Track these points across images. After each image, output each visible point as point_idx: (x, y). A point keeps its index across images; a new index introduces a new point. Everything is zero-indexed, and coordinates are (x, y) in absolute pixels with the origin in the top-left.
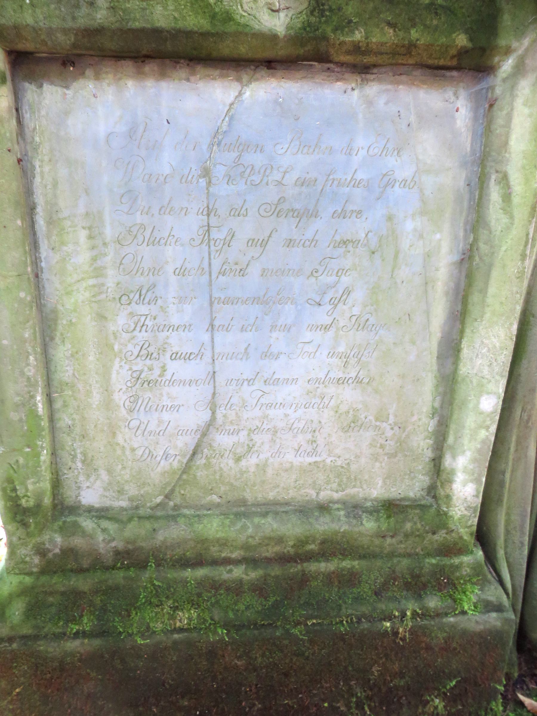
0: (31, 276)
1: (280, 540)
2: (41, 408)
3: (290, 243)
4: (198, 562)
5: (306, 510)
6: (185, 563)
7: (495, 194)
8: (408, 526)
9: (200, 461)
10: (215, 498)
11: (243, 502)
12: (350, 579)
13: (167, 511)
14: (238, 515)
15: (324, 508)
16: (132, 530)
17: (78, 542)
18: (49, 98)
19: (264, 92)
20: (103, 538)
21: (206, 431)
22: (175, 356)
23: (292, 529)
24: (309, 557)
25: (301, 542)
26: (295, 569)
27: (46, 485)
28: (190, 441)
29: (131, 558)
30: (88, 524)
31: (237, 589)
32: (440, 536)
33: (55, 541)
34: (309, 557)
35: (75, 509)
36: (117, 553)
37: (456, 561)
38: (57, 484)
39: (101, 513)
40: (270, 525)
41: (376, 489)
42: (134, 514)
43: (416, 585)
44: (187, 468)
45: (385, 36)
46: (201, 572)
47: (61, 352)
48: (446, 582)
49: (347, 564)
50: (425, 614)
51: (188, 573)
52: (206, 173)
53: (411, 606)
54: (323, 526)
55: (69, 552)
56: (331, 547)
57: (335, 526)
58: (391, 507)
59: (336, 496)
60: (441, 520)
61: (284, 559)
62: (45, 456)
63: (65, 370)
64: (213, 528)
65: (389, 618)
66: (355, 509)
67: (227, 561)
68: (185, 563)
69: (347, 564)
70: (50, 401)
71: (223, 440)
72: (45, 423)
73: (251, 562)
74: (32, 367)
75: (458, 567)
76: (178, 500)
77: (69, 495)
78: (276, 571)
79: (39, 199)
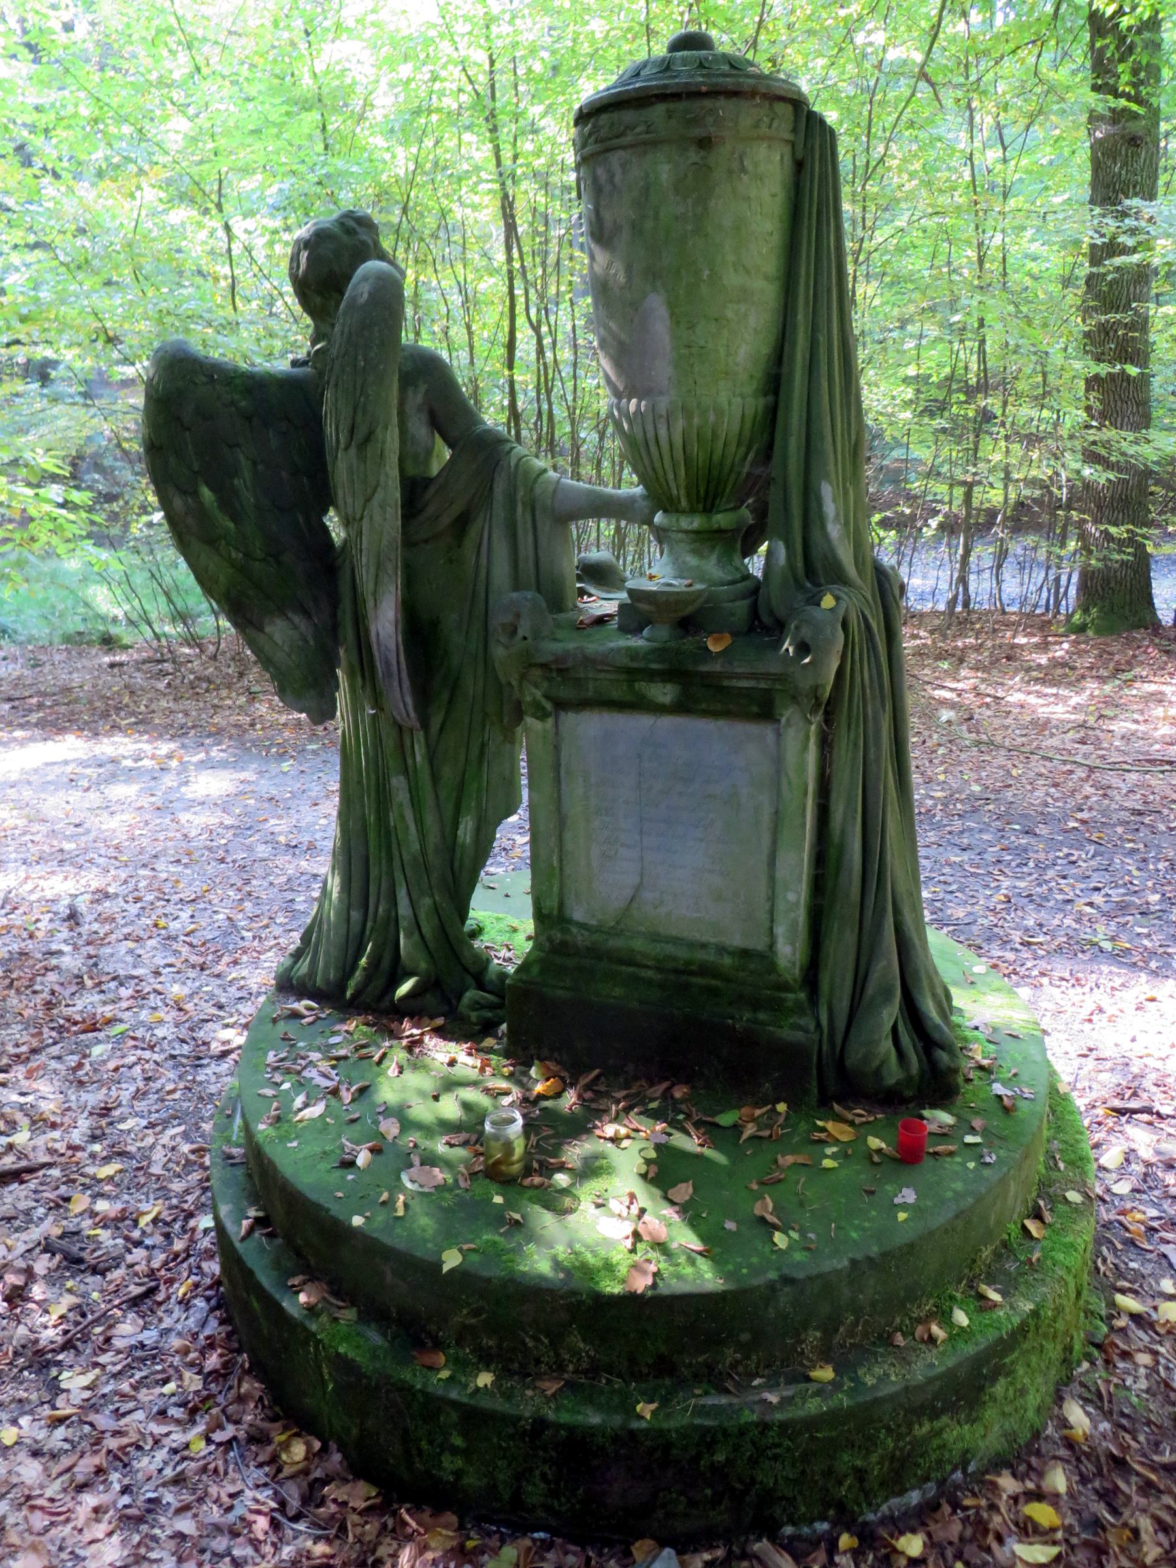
0: (730, 258)
1: (675, 959)
2: (555, 863)
3: (681, 794)
4: (630, 963)
5: (692, 945)
6: (622, 962)
7: (784, 782)
8: (752, 966)
9: (634, 905)
10: (643, 929)
11: (659, 935)
12: (713, 992)
13: (616, 931)
14: (654, 941)
15: (704, 946)
16: (596, 937)
17: (568, 938)
18: (570, 719)
19: (667, 722)
20: (580, 938)
21: (638, 888)
22: (623, 845)
23: (683, 954)
24: (692, 973)
25: (688, 963)
26: (684, 978)
27: (556, 905)
28: (629, 892)
29: (594, 952)
30: (574, 930)
31: (649, 982)
32: (773, 977)
33: (558, 936)
34: (692, 973)
35: (570, 921)
36: (588, 949)
37: (783, 995)
38: (561, 905)
39: (583, 926)
40: (669, 949)
41: (737, 941)
42: (598, 929)
43: (756, 1005)
44: (628, 908)
45: (719, 707)
46: (631, 969)
47: (568, 835)
48: (776, 1007)
49: (714, 982)
50: (755, 1021)
51: (623, 968)
52: (639, 756)
53: (747, 1016)
54: (701, 955)
55: (564, 944)
56: (705, 970)
57: (706, 957)
58: (745, 953)
59: (712, 940)
60: (772, 967)
61: (676, 971)
62: (555, 889)
63: (569, 846)
64: (638, 944)
65: (732, 1018)
66: (722, 950)
67: (646, 967)
68: (622, 962)
69: (714, 982)
70: (561, 860)
71: (648, 895)
72: (557, 871)
73: (659, 969)
74: (553, 841)
75: (785, 1000)
76: (622, 926)
77: (568, 913)
78: (672, 977)
79: (563, 763)
